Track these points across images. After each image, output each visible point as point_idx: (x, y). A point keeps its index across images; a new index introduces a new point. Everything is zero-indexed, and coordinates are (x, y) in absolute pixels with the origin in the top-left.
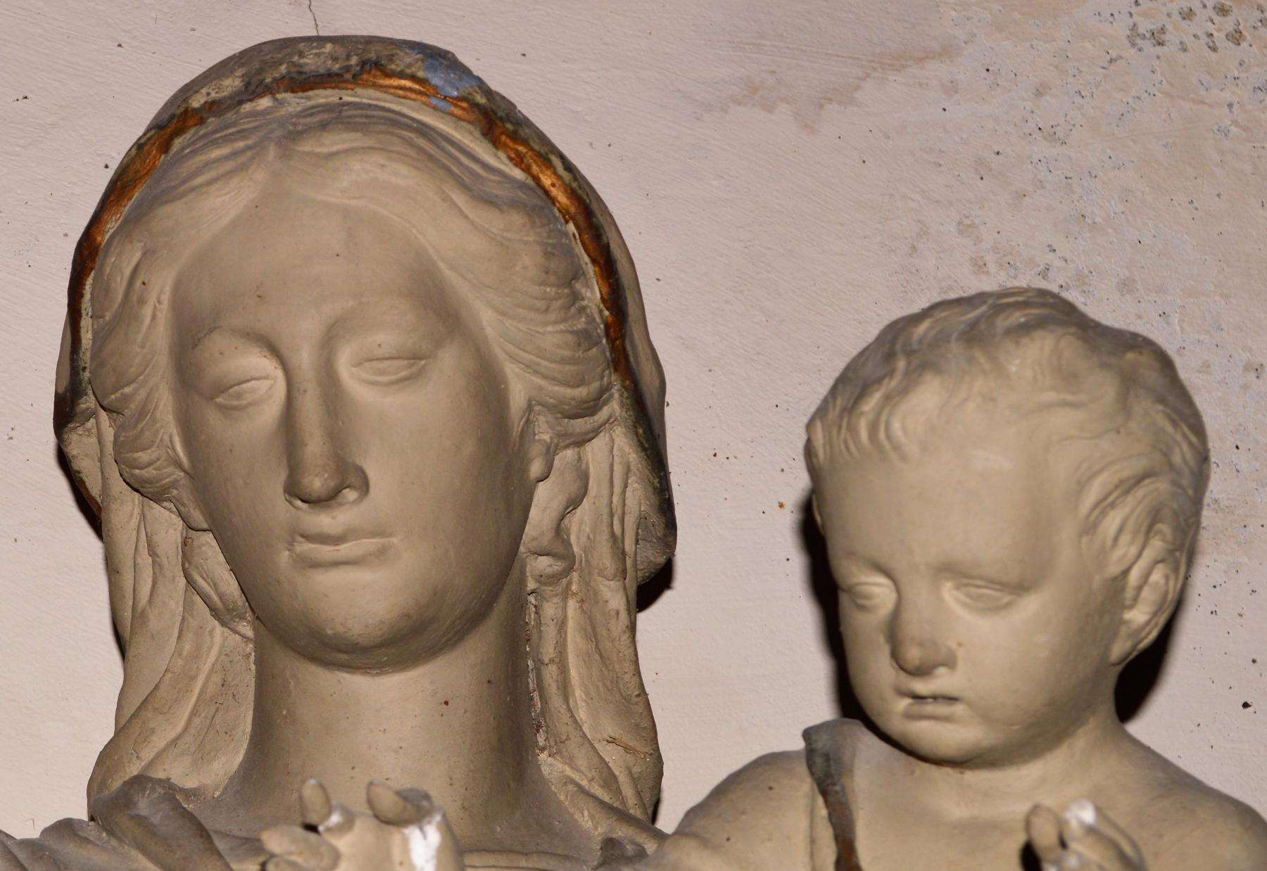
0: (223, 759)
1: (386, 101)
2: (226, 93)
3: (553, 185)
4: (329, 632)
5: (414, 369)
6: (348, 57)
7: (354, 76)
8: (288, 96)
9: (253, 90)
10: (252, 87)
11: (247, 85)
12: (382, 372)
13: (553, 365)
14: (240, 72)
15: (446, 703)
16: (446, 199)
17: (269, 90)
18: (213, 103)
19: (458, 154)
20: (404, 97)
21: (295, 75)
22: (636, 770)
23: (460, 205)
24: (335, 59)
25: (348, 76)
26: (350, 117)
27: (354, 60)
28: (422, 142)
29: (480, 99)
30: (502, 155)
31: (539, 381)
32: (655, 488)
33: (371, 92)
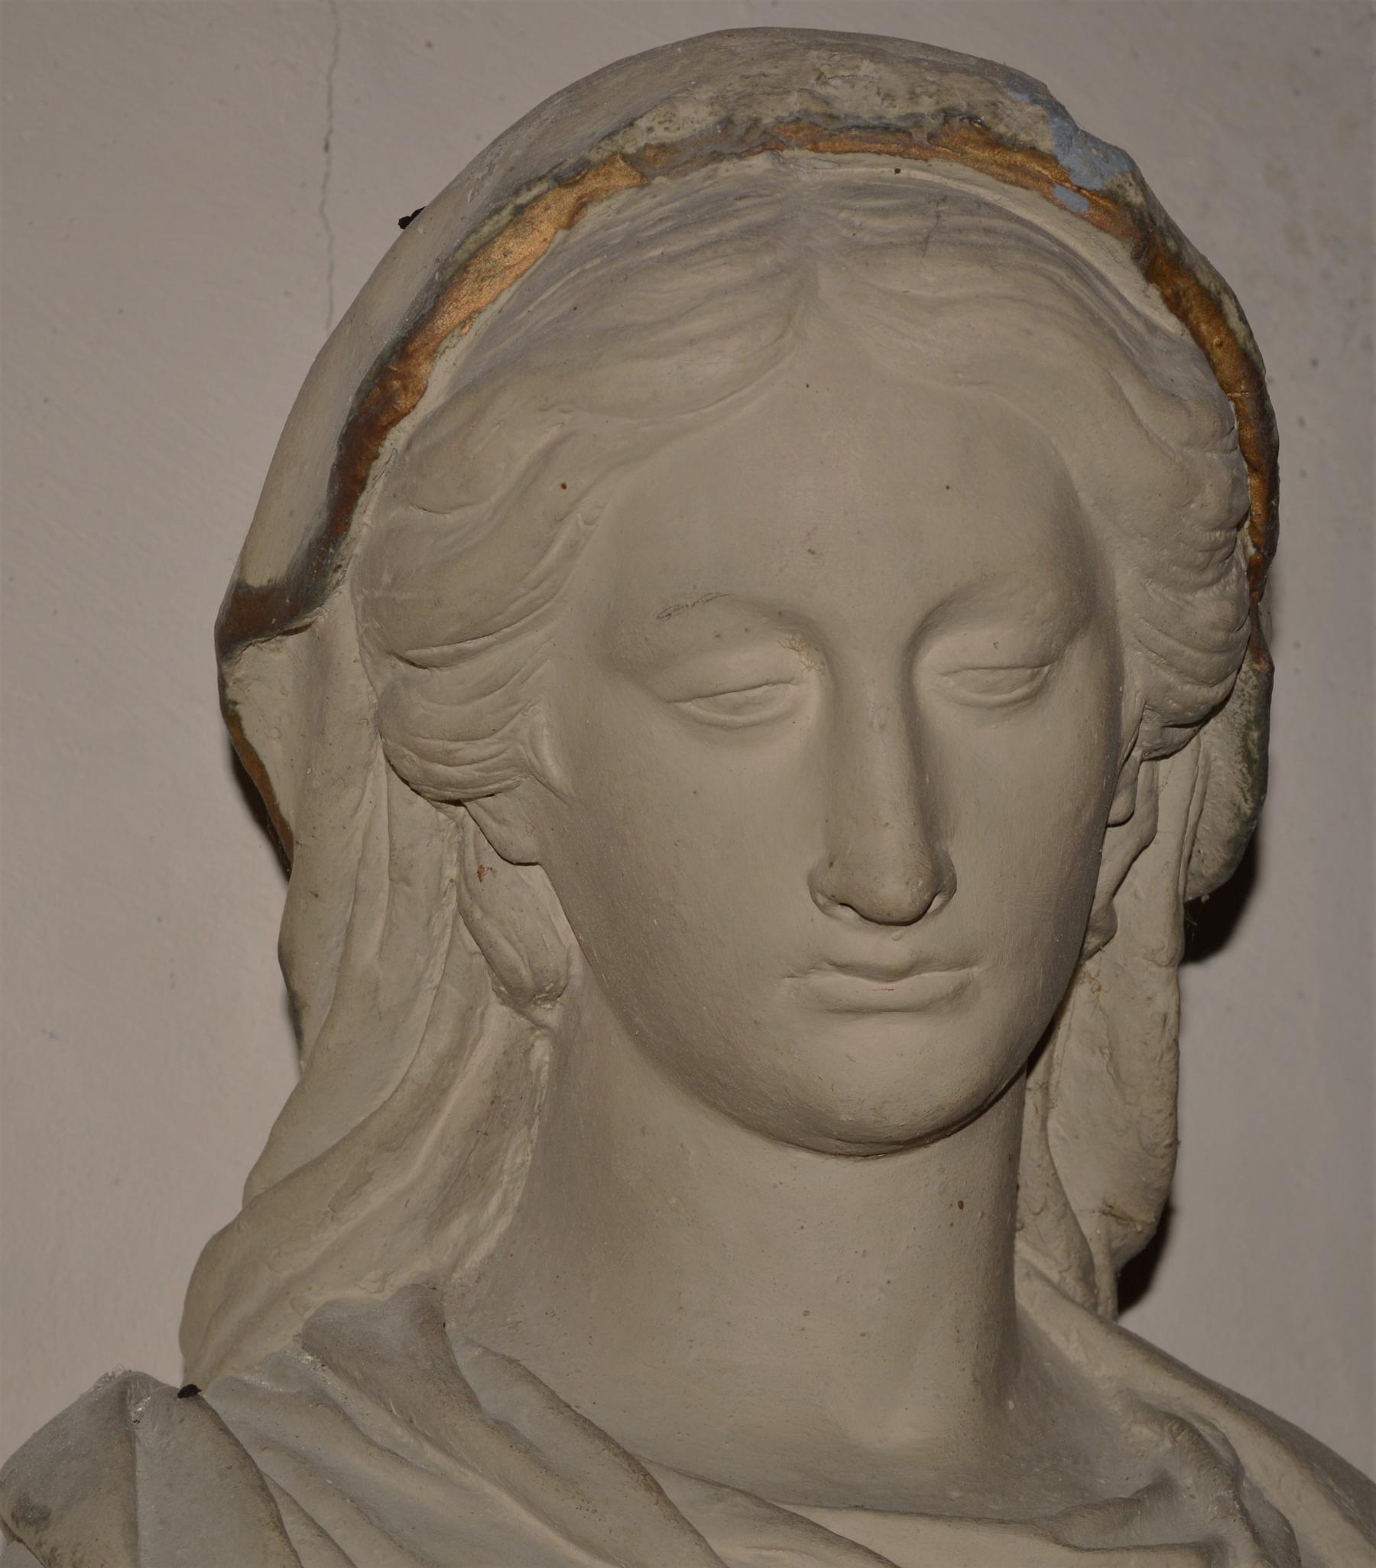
0: (465, 1218)
1: (972, 183)
2: (685, 133)
3: (1220, 345)
4: (843, 1117)
5: (1036, 683)
6: (913, 97)
7: (931, 136)
8: (803, 155)
9: (737, 137)
10: (739, 131)
11: (727, 123)
12: (990, 689)
13: (1198, 655)
14: (705, 92)
15: (961, 1205)
16: (1116, 392)
17: (771, 142)
18: (662, 147)
19: (1116, 302)
20: (1015, 183)
21: (819, 120)
22: (1115, 1244)
23: (1132, 399)
24: (889, 96)
25: (920, 137)
26: (960, 230)
27: (926, 106)
28: (1074, 285)
29: (1135, 197)
30: (1154, 292)
31: (1168, 677)
32: (1238, 815)
33: (957, 167)
